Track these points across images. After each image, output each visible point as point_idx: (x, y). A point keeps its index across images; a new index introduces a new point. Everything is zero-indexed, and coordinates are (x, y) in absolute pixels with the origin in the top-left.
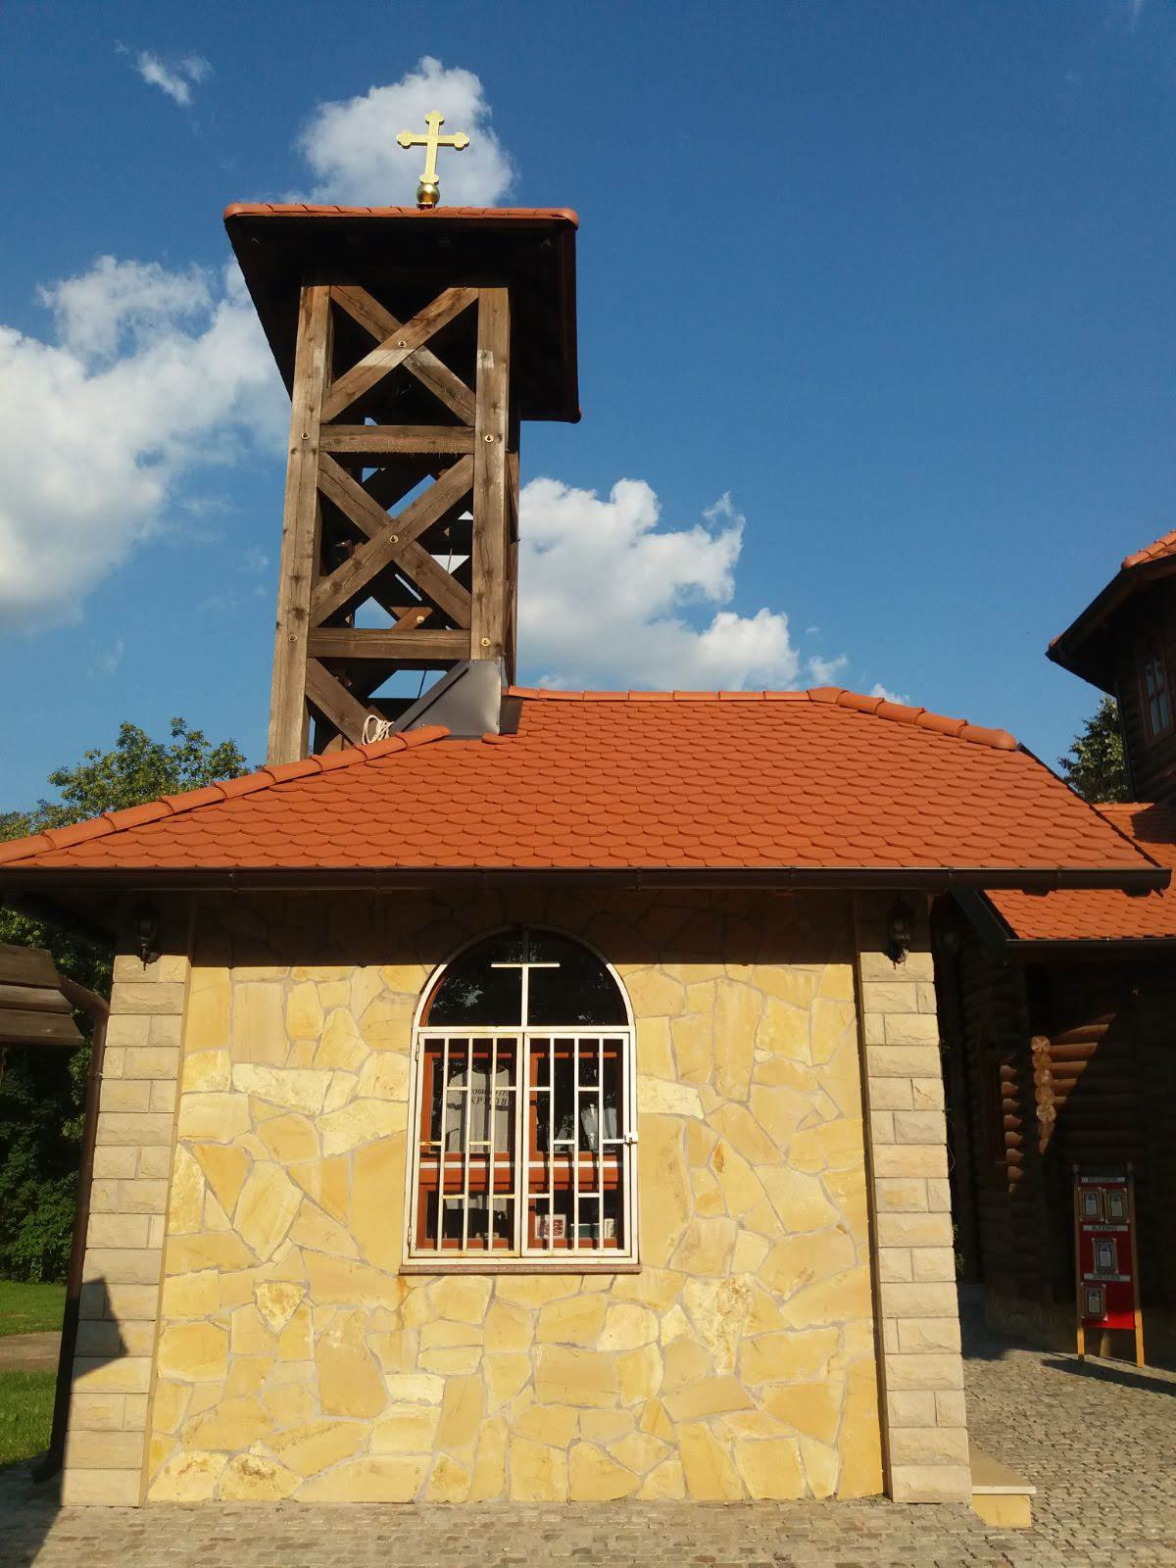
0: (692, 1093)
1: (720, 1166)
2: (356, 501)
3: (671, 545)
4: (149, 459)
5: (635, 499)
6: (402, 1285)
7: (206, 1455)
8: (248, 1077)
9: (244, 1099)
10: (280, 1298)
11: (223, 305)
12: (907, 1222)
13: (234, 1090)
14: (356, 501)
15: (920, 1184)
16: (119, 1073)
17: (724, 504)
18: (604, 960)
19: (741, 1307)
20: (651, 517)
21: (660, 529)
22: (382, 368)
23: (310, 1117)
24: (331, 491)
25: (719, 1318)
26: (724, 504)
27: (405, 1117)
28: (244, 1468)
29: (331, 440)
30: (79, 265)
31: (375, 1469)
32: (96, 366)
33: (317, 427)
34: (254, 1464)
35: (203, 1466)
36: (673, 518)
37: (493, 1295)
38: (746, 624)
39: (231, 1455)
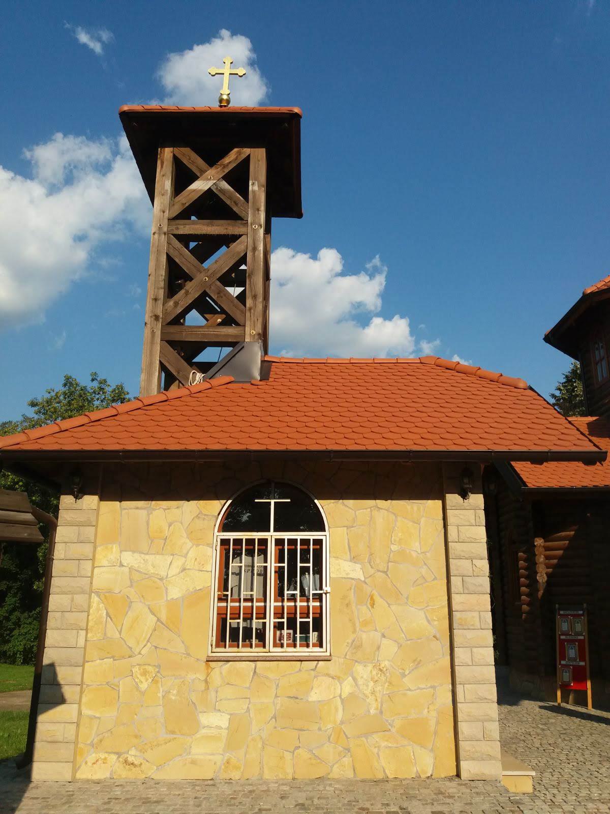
0: (358, 566)
1: (373, 605)
2: (186, 260)
3: (349, 282)
4: (80, 238)
5: (330, 258)
6: (208, 666)
7: (106, 755)
8: (129, 558)
9: (126, 570)
10: (144, 673)
11: (118, 158)
12: (470, 634)
13: (122, 565)
14: (186, 260)
15: (476, 614)
16: (62, 557)
17: (377, 261)
18: (313, 497)
19: (383, 678)
20: (339, 268)
21: (343, 274)
22: (200, 190)
23: (161, 579)
24: (174, 255)
25: (371, 684)
26: (377, 261)
27: (210, 579)
28: (126, 761)
29: (174, 227)
30: (44, 138)
31: (193, 762)
32: (53, 189)
33: (166, 221)
34: (130, 759)
35: (105, 761)
36: (350, 268)
37: (255, 672)
38: (388, 323)
39: (119, 754)
